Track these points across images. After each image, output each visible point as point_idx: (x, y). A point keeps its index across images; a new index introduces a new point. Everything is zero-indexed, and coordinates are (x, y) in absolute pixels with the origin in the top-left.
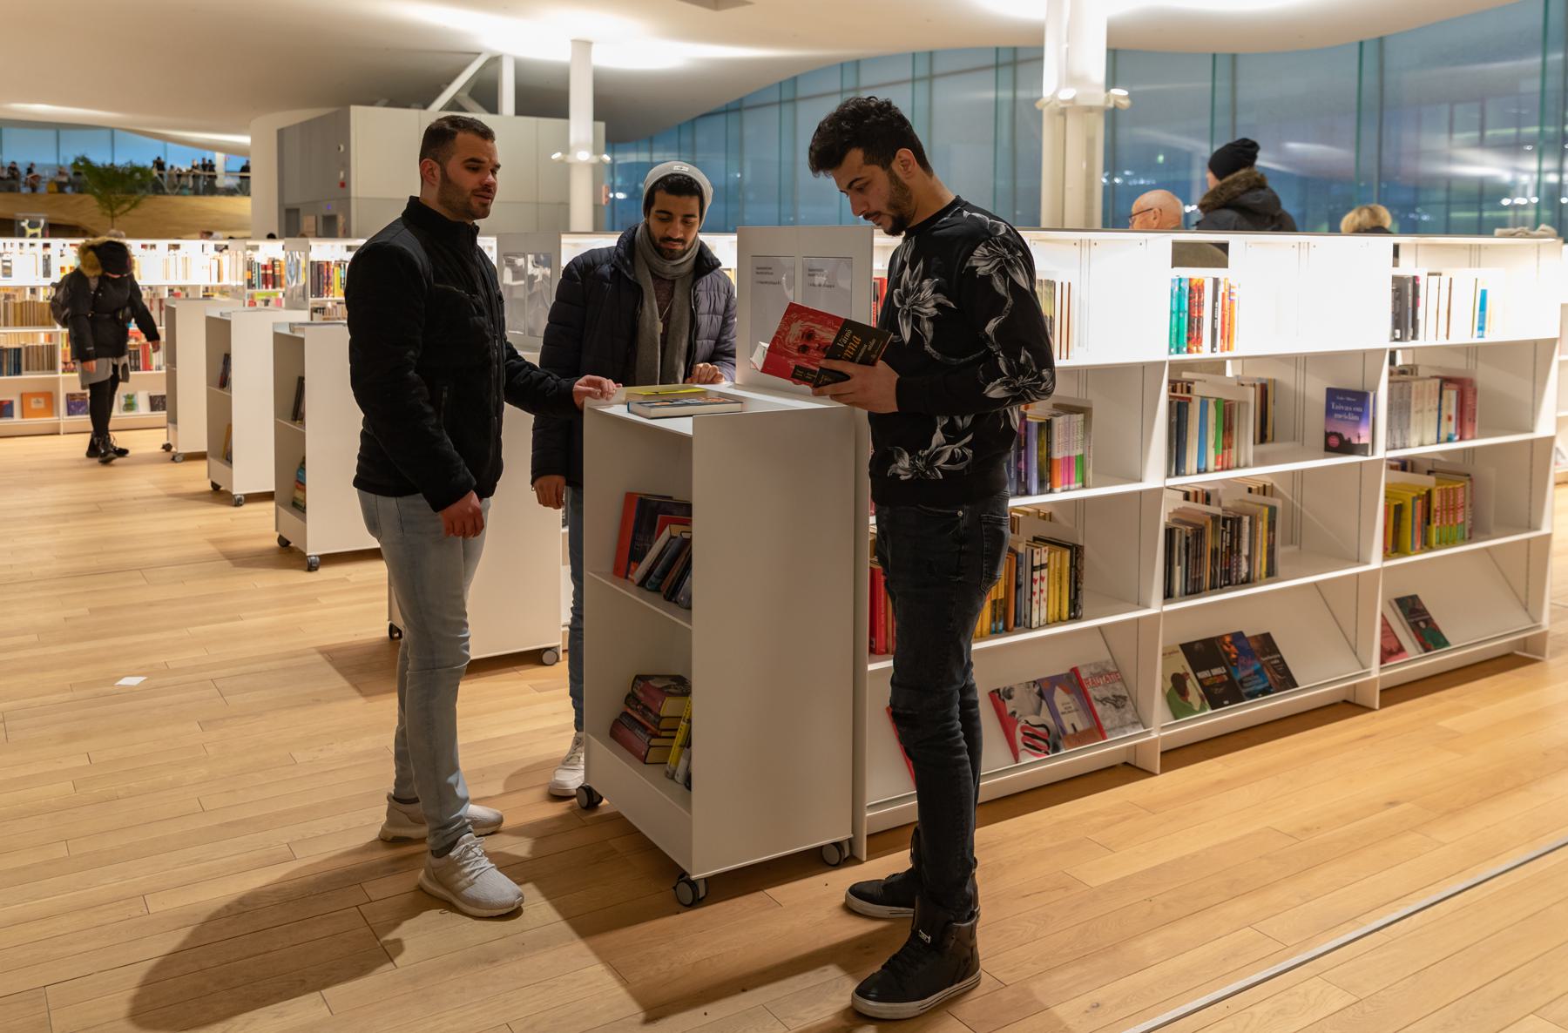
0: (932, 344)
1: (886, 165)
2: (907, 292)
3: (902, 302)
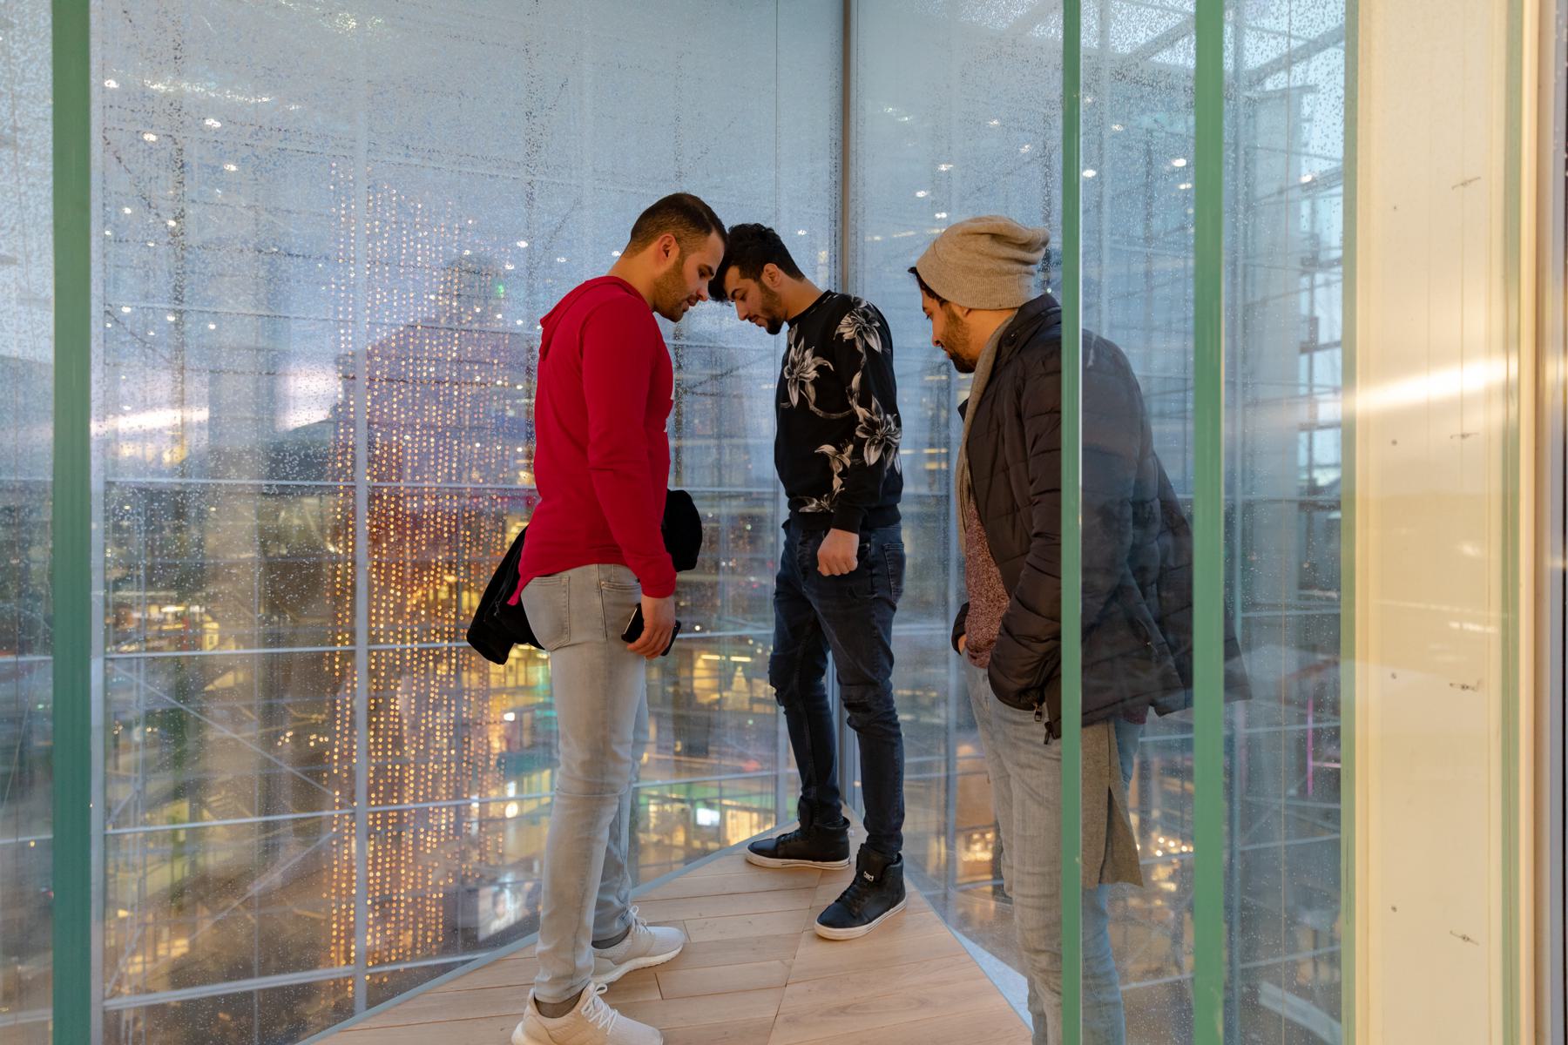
0: (816, 404)
1: (757, 277)
2: (794, 365)
3: (790, 373)
